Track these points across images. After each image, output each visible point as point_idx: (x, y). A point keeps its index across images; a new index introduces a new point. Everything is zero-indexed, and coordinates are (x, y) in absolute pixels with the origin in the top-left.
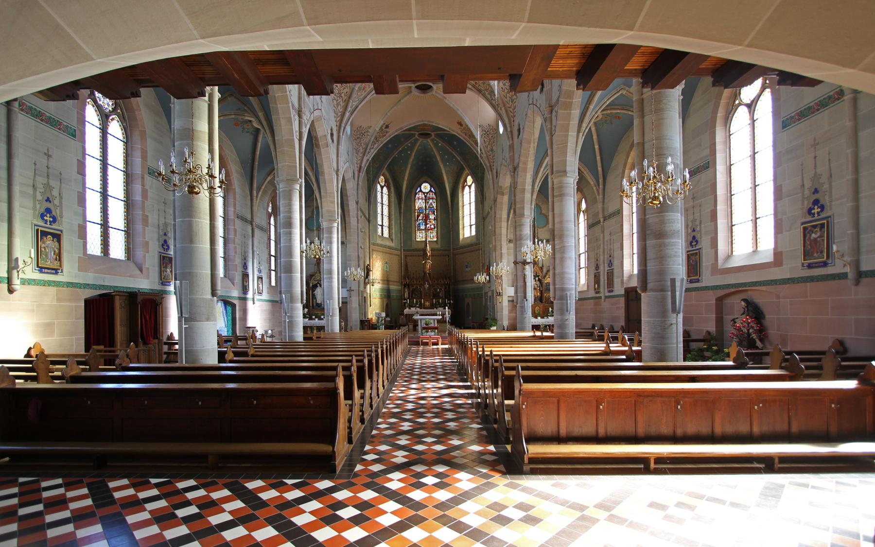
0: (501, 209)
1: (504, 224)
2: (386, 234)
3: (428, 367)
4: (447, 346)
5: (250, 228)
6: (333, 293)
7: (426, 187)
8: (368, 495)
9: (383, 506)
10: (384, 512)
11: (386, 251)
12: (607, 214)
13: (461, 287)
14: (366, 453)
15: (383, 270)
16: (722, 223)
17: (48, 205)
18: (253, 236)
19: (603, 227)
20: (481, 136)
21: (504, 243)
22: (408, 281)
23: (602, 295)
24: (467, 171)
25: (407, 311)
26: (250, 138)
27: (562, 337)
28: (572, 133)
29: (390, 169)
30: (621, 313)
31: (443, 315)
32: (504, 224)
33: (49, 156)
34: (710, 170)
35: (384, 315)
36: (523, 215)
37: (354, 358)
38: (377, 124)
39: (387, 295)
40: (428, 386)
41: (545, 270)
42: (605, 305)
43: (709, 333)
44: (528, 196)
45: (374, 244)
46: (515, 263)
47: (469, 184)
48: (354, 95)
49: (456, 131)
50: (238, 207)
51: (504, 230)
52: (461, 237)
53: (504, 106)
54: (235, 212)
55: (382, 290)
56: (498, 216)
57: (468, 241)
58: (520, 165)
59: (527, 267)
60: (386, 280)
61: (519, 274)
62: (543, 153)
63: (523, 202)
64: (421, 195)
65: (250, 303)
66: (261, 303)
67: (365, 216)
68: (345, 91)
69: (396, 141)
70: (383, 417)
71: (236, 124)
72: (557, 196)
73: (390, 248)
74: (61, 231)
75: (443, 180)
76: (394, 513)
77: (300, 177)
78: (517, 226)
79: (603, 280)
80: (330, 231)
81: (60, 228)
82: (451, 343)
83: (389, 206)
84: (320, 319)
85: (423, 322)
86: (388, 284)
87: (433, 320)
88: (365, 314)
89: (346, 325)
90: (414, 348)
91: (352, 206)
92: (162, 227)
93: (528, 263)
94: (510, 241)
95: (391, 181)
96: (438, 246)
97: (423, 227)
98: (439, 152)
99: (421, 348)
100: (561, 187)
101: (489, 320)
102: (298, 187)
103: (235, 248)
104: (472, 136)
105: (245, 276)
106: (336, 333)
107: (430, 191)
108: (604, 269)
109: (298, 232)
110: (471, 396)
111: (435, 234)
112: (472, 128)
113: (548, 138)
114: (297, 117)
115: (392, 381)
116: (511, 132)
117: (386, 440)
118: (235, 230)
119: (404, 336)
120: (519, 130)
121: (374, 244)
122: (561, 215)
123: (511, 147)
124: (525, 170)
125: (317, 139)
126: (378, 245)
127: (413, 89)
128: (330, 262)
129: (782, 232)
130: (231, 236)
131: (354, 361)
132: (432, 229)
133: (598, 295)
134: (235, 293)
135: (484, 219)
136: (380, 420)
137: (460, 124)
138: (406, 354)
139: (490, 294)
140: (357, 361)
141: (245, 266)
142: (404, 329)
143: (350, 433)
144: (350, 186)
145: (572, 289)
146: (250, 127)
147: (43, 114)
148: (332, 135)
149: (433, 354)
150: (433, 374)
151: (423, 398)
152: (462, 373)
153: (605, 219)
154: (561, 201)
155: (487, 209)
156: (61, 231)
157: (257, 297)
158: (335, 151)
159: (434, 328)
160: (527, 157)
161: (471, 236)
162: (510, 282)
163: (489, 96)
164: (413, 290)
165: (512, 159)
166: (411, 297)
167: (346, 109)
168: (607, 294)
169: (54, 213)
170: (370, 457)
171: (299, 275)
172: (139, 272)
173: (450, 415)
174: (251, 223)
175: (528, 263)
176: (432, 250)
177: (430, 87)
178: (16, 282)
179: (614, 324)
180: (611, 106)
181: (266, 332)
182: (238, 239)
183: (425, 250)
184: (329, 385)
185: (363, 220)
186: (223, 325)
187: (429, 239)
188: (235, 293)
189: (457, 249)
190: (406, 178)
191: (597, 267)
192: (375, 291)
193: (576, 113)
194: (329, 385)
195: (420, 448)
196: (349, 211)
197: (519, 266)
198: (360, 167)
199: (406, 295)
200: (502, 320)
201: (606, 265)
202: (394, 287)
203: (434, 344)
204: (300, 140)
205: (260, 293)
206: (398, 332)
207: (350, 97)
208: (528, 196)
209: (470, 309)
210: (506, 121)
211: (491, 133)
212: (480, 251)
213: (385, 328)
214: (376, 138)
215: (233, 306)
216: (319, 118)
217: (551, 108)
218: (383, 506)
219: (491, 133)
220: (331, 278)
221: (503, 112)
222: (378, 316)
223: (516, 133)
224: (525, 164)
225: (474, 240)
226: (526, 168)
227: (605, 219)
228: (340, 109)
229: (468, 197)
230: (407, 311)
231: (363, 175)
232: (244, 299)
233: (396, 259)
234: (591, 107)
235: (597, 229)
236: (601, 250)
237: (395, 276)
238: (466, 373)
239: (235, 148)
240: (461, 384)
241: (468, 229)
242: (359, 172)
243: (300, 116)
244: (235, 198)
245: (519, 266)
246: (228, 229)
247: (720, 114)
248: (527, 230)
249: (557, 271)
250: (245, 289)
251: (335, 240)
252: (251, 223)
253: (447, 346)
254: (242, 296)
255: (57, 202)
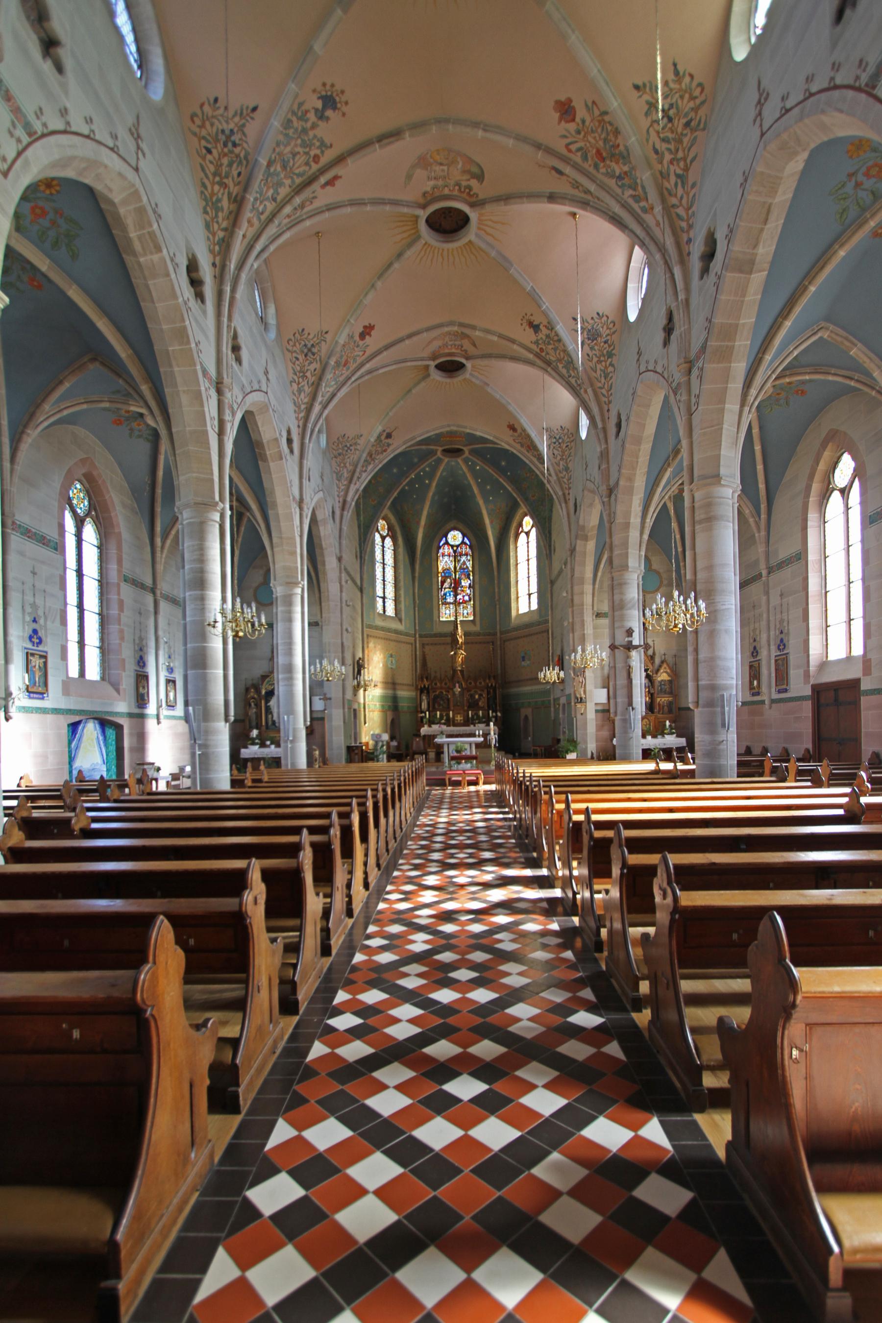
0: (583, 564)
1: (588, 588)
2: (390, 611)
3: (461, 832)
4: (493, 787)
5: (150, 599)
6: (295, 704)
7: (455, 537)
8: (373, 997)
9: (395, 1012)
10: (396, 1021)
11: (390, 636)
12: (773, 562)
13: (514, 690)
14: (337, 1012)
15: (385, 666)
16: (814, 621)
17: (35, 626)
18: (156, 613)
19: (767, 586)
20: (549, 446)
21: (588, 618)
22: (426, 683)
23: (765, 697)
24: (523, 508)
25: (425, 730)
26: (143, 448)
27: (713, 775)
28: (732, 407)
29: (394, 507)
30: (806, 728)
31: (486, 735)
32: (588, 588)
33: (34, 573)
34: (803, 562)
35: (386, 737)
36: (625, 567)
37: (354, 801)
38: (372, 431)
39: (392, 705)
40: (462, 880)
41: (657, 661)
42: (771, 714)
43: (807, 750)
44: (634, 534)
45: (370, 627)
46: (613, 647)
47: (526, 529)
48: (329, 376)
49: (506, 442)
50: (126, 564)
51: (589, 598)
52: (514, 613)
53: (592, 385)
54: (119, 572)
55: (384, 698)
56: (577, 574)
57: (526, 620)
58: (621, 483)
59: (634, 653)
60: (391, 683)
61: (620, 665)
62: (667, 453)
63: (625, 544)
64: (447, 550)
65: (151, 724)
66: (174, 722)
67: (357, 586)
68: (312, 367)
69: (404, 462)
70: (377, 922)
71: (118, 422)
72: (700, 522)
73: (396, 632)
74: (46, 652)
75: (484, 525)
76: (412, 1021)
77: (222, 499)
78: (616, 587)
79: (768, 672)
80: (288, 601)
81: (45, 649)
82: (499, 782)
83: (396, 568)
84: (278, 745)
85: (452, 747)
86: (394, 689)
87: (468, 744)
88: (356, 736)
89: (323, 754)
90: (437, 791)
91: (331, 564)
92: (137, 641)
93: (636, 647)
94: (598, 615)
95: (397, 529)
96: (477, 628)
97: (450, 599)
98: (476, 479)
99: (449, 790)
100: (710, 504)
101: (562, 743)
102: (217, 517)
103: (121, 631)
104: (532, 447)
105: (142, 679)
106: (299, 771)
107: (463, 542)
108: (768, 656)
109: (218, 599)
110: (551, 908)
111: (470, 609)
112: (533, 434)
113: (607, 525)
114: (213, 393)
115: (387, 869)
116: (604, 429)
117: (380, 977)
118: (121, 603)
119: (417, 774)
120: (619, 426)
121: (370, 627)
122: (710, 553)
123: (604, 455)
124: (630, 491)
125: (260, 444)
126: (377, 628)
127: (432, 370)
128: (290, 652)
129: (870, 638)
130: (114, 611)
131: (335, 817)
132: (465, 602)
133: (756, 698)
134: (122, 707)
135: (552, 583)
136: (389, 888)
137: (512, 428)
138: (419, 807)
139: (563, 700)
140: (359, 804)
141: (141, 662)
142: (420, 760)
143: (350, 903)
144: (328, 532)
145: (731, 687)
146: (143, 427)
147: (30, 531)
148: (290, 441)
149: (469, 803)
150: (468, 848)
151: (448, 916)
152: (526, 846)
153: (770, 571)
154: (710, 529)
155: (556, 566)
156: (46, 652)
157: (164, 712)
158: (297, 470)
159: (469, 758)
160: (634, 469)
161: (530, 612)
162: (599, 681)
163: (564, 371)
164: (436, 697)
165: (606, 475)
166: (432, 708)
167: (314, 397)
168: (775, 696)
169: (40, 634)
170: (345, 1022)
171: (221, 672)
172: (115, 694)
173: (483, 838)
174: (153, 591)
175: (636, 647)
176: (466, 634)
177: (461, 366)
178: (162, 717)
179: (791, 747)
180: (791, 369)
181: (182, 769)
182: (127, 618)
183: (454, 635)
184: (226, 904)
185: (351, 591)
186: (98, 759)
187: (460, 618)
188: (122, 707)
189: (508, 632)
190: (423, 522)
191: (755, 652)
192: (372, 698)
193: (740, 367)
194: (226, 904)
195: (445, 996)
196: (325, 573)
197: (619, 653)
198: (345, 502)
199: (424, 705)
200: (586, 742)
201: (773, 648)
202: (404, 694)
203: (471, 783)
204: (301, 536)
205: (171, 706)
206: (406, 767)
207: (320, 379)
208: (634, 534)
209: (528, 726)
210: (595, 410)
211: (566, 439)
212: (547, 634)
213: (389, 761)
214: (370, 454)
215: (119, 728)
216: (265, 408)
217: (690, 365)
218: (395, 1012)
219: (566, 439)
220: (290, 679)
221: (590, 396)
222: (376, 738)
223: (612, 430)
224: (631, 479)
225: (536, 617)
226: (632, 488)
227: (770, 571)
228: (304, 398)
229: (525, 550)
230: (425, 730)
231: (349, 514)
232: (139, 717)
233: (406, 652)
234: (768, 357)
235: (755, 589)
236: (764, 623)
237: (406, 676)
238: (538, 848)
239: (120, 465)
240: (528, 872)
241: (525, 598)
242: (343, 509)
243: (219, 392)
244: (119, 548)
245: (619, 653)
246: (108, 600)
247: (813, 499)
248: (633, 593)
249: (702, 656)
250: (141, 700)
251: (297, 616)
252: (153, 591)
253: (493, 787)
254: (137, 711)
255: (42, 621)
